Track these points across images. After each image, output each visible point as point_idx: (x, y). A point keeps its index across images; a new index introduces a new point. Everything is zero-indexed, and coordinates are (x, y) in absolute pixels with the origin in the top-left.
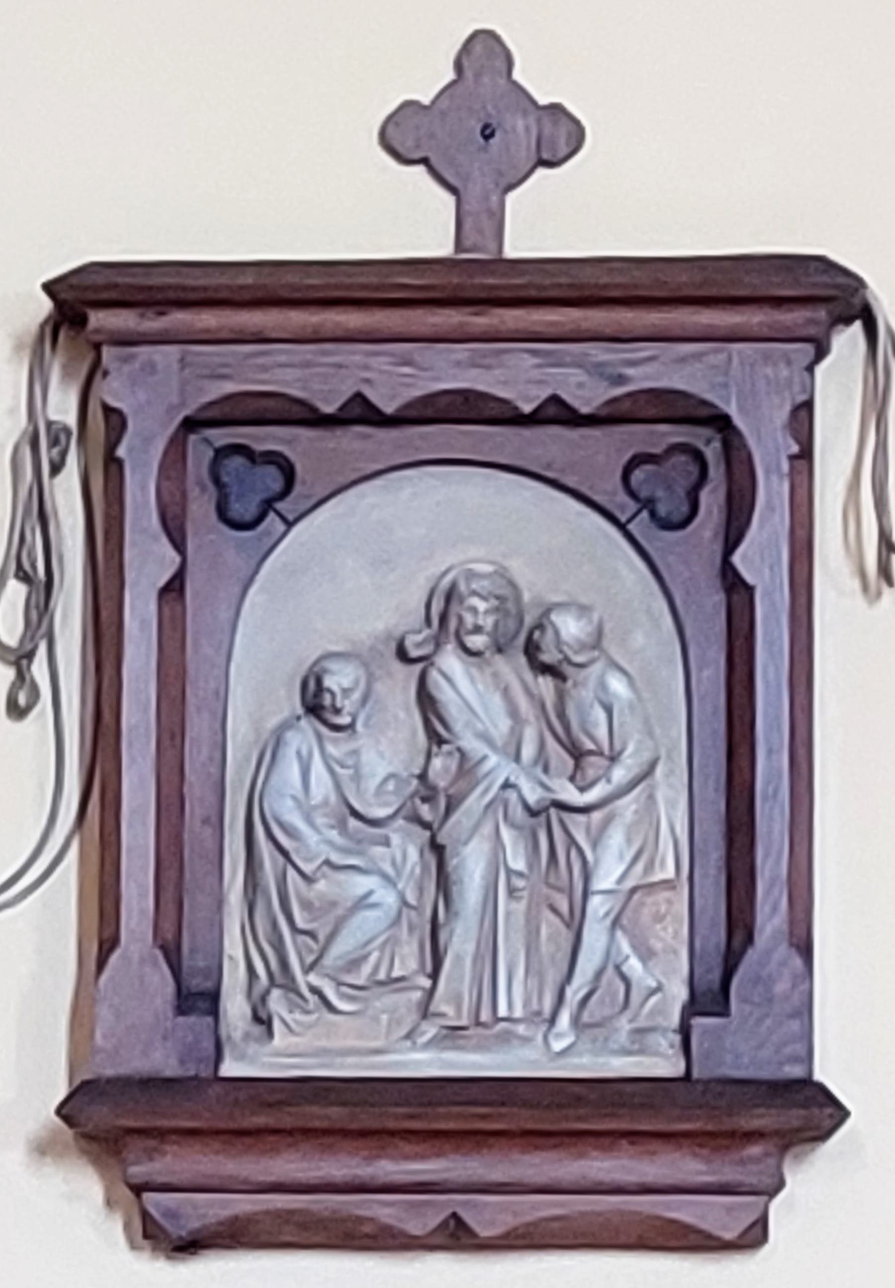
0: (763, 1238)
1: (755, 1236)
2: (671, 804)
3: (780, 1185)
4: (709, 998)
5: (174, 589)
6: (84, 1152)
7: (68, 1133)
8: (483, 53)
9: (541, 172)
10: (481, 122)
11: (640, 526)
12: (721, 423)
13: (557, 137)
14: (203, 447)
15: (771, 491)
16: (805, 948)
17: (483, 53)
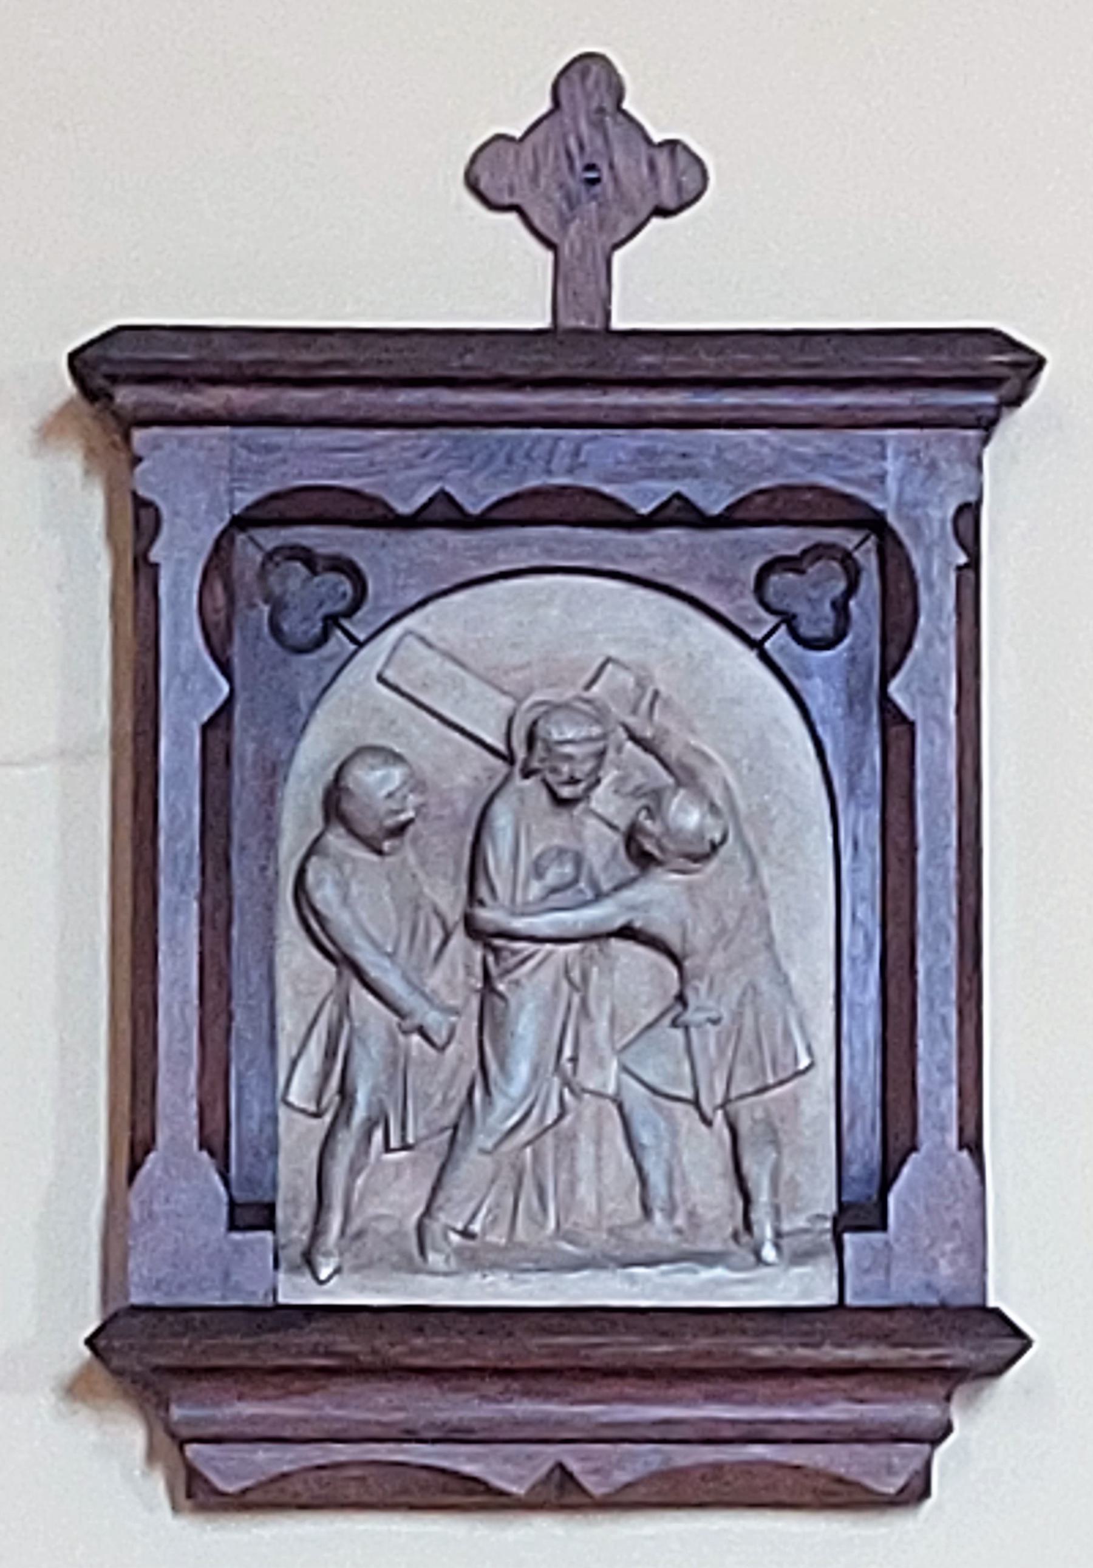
0: (926, 1492)
1: (917, 1491)
2: (340, 1452)
3: (948, 1429)
4: (861, 1211)
5: (219, 722)
6: (126, 1395)
7: (100, 1373)
8: (588, 83)
9: (656, 222)
10: (586, 160)
11: (779, 642)
12: (875, 524)
13: (676, 180)
14: (251, 549)
15: (937, 600)
16: (972, 1144)
17: (588, 83)
